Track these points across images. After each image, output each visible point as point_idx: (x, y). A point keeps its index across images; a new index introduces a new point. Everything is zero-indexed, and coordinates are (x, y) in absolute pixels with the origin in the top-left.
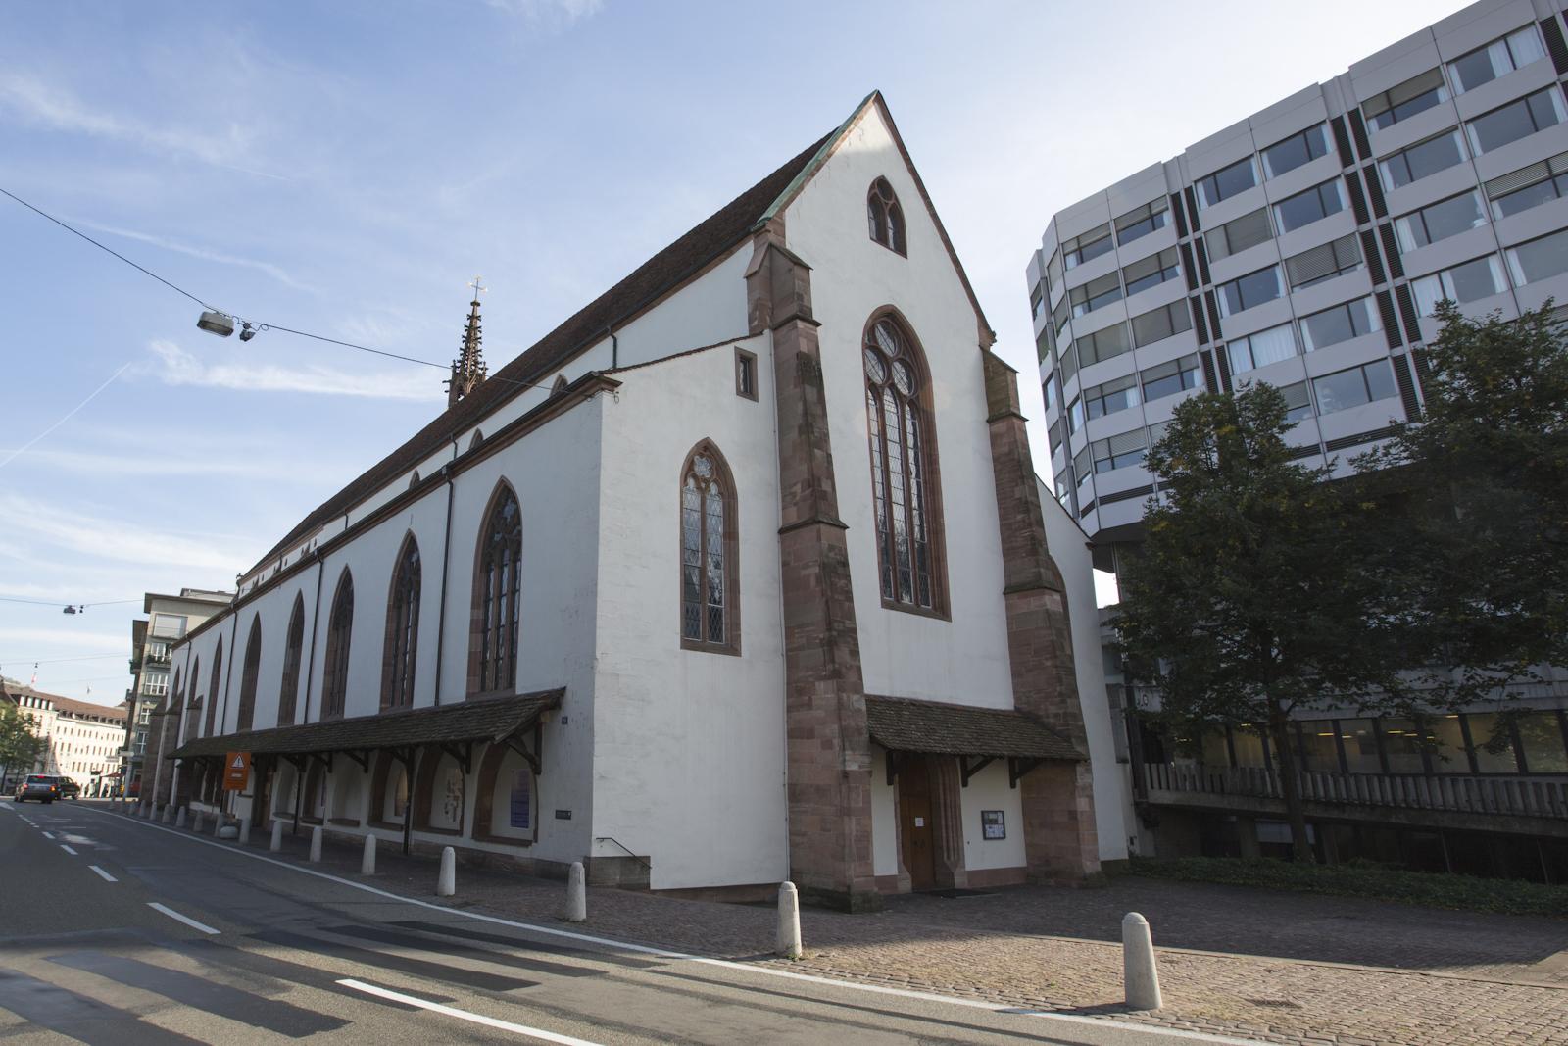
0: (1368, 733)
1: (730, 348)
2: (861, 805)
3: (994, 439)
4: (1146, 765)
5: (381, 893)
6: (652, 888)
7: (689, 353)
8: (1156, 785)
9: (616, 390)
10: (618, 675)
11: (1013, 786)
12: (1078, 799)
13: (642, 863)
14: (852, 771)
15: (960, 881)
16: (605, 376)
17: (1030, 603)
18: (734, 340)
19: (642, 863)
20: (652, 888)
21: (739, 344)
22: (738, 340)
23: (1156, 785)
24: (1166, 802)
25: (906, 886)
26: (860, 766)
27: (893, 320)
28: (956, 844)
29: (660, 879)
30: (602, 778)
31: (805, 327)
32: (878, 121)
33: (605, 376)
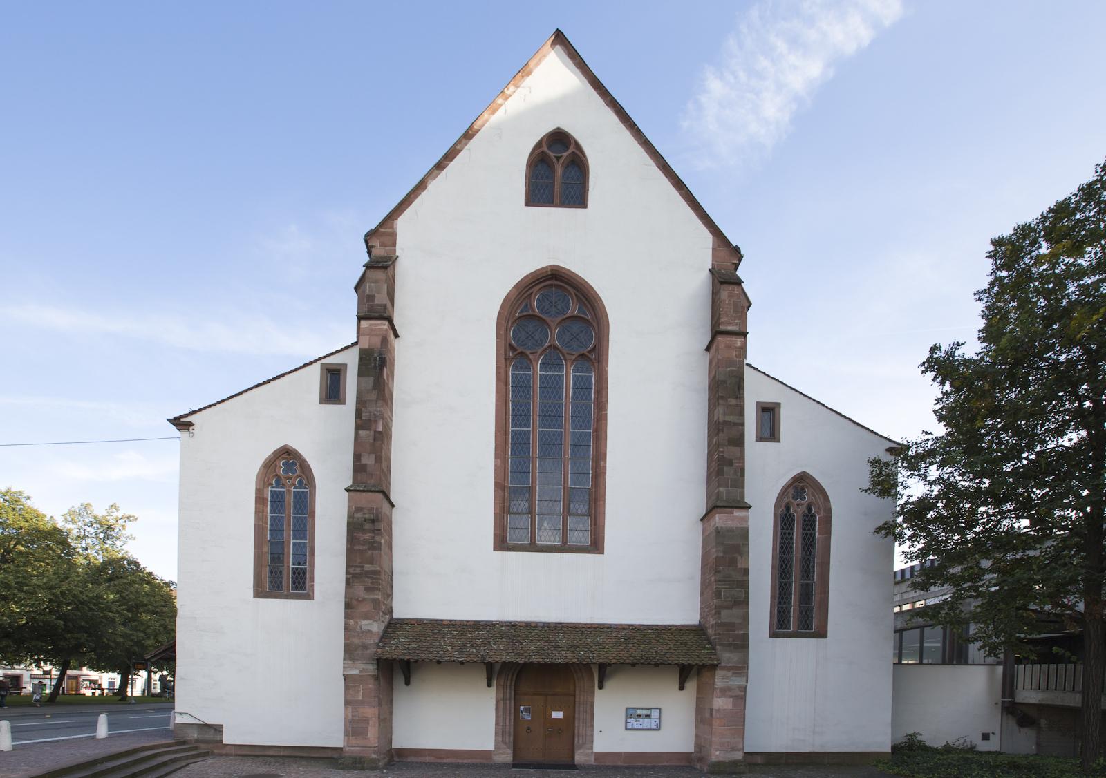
0: (1080, 598)
1: (317, 366)
2: (360, 698)
3: (713, 366)
4: (1016, 666)
5: (72, 737)
6: (224, 743)
7: (268, 382)
8: (1028, 685)
9: (191, 428)
10: (195, 618)
11: (489, 685)
12: (715, 699)
13: (218, 729)
14: (714, 676)
15: (579, 758)
16: (182, 420)
17: (719, 520)
18: (320, 359)
19: (218, 729)
20: (224, 743)
21: (324, 361)
22: (324, 357)
23: (1028, 685)
24: (1032, 701)
25: (506, 756)
26: (361, 672)
27: (556, 279)
28: (584, 732)
29: (228, 738)
30: (182, 679)
31: (371, 325)
32: (561, 65)
33: (182, 420)
